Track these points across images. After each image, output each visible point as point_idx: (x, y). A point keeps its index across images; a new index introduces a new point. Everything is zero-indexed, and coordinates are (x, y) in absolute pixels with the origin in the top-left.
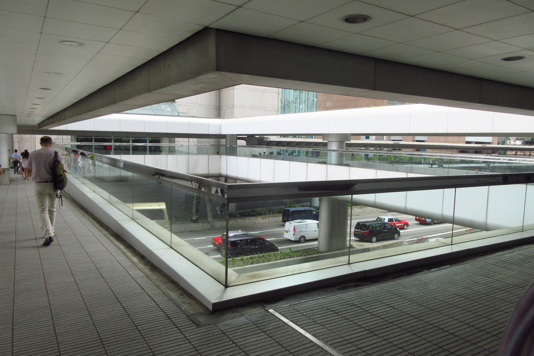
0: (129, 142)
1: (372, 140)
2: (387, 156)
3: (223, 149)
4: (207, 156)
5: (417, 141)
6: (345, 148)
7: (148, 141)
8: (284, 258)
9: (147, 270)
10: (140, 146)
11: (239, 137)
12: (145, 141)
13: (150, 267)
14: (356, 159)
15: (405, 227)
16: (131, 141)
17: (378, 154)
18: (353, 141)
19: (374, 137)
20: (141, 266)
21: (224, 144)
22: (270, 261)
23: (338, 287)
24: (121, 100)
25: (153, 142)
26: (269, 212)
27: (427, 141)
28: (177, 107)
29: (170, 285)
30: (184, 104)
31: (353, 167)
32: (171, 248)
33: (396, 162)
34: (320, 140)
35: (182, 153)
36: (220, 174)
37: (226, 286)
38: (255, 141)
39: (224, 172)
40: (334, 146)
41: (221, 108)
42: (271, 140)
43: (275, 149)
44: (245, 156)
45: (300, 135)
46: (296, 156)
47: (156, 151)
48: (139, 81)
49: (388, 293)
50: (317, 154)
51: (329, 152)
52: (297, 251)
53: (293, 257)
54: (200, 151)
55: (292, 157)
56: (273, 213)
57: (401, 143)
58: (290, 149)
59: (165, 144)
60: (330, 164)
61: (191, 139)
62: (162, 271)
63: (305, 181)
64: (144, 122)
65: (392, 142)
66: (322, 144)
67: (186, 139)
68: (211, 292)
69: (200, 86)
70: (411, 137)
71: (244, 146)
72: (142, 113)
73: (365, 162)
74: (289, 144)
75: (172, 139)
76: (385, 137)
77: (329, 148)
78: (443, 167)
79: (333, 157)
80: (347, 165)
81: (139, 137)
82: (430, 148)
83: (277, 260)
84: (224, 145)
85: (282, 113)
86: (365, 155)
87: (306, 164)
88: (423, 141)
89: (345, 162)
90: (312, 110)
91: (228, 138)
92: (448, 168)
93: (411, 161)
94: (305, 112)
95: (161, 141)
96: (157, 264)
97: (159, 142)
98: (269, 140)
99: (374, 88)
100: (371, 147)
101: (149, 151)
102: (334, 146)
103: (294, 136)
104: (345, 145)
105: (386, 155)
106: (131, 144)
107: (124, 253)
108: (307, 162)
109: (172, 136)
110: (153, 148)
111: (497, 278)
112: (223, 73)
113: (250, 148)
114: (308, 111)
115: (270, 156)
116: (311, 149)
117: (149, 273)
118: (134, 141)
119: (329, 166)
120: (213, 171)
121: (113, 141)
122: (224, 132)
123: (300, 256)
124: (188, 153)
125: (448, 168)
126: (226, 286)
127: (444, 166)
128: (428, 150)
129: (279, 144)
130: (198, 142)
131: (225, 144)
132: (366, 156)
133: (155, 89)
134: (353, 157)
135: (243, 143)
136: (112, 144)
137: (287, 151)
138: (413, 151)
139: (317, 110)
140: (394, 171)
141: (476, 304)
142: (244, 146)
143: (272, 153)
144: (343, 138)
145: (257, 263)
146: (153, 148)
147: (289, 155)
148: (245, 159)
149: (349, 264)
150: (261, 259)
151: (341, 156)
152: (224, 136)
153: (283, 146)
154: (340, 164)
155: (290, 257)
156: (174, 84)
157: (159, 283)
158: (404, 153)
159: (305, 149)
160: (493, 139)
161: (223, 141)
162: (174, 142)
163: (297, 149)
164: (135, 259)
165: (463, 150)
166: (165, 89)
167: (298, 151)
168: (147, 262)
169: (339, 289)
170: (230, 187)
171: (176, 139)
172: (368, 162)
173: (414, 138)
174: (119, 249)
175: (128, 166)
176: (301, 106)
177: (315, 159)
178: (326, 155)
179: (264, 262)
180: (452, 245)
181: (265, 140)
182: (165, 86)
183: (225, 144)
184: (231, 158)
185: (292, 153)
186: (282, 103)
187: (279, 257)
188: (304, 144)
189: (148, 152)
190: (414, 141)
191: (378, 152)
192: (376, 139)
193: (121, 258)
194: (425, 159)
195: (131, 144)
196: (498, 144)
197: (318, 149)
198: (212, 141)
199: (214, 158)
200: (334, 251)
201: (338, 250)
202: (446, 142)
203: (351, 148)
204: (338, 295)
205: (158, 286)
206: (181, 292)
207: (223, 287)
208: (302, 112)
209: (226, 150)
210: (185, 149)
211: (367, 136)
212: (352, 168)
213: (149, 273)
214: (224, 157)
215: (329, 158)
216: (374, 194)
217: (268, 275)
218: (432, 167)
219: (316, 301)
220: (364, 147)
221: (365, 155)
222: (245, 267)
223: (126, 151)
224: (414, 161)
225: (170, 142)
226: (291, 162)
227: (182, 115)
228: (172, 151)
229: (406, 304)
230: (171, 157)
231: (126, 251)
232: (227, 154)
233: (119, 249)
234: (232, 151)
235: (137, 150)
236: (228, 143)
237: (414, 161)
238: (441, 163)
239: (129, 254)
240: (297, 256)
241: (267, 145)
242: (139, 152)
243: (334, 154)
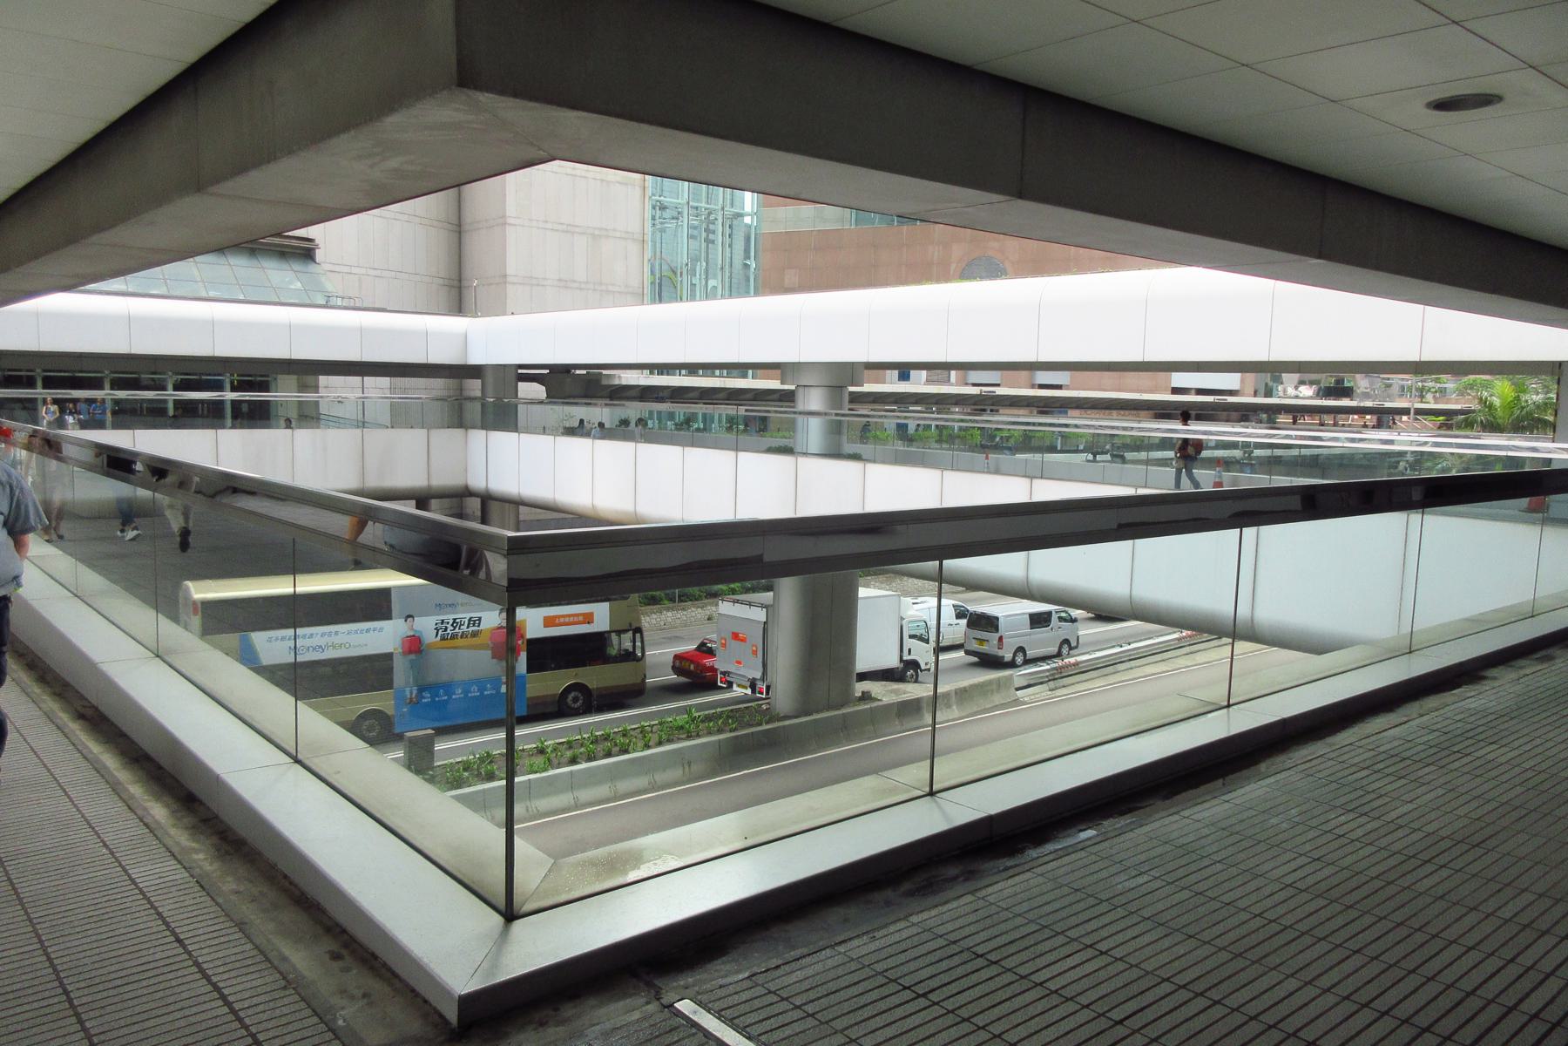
0: (164, 389)
1: (919, 384)
2: (961, 429)
3: (473, 410)
4: (424, 431)
5: (1042, 386)
6: (846, 405)
7: (228, 386)
8: (670, 741)
9: (202, 857)
10: (202, 401)
11: (523, 373)
12: (218, 386)
13: (215, 839)
14: (876, 437)
15: (1065, 650)
16: (170, 386)
17: (934, 423)
18: (868, 388)
19: (924, 373)
20: (180, 837)
21: (477, 396)
22: (626, 752)
23: (906, 886)
24: (99, 228)
25: (246, 390)
27: (1068, 388)
28: (323, 279)
29: (291, 915)
30: (346, 269)
31: (874, 462)
32: (297, 761)
33: (989, 447)
34: (774, 384)
35: (339, 422)
36: (467, 487)
37: (510, 915)
38: (576, 386)
39: (477, 482)
40: (814, 400)
41: (465, 283)
43: (633, 410)
44: (544, 431)
45: (709, 368)
46: (698, 430)
47: (255, 416)
48: (160, 149)
49: (1079, 895)
50: (761, 425)
51: (800, 419)
52: (708, 719)
53: (698, 736)
54: (401, 417)
55: (688, 432)
57: (1000, 391)
58: (681, 410)
59: (283, 394)
60: (805, 454)
61: (370, 381)
62: (260, 854)
63: (792, 515)
64: (212, 325)
65: (975, 391)
66: (776, 396)
67: (355, 380)
68: (455, 949)
69: (394, 163)
70: (1024, 374)
71: (541, 402)
72: (204, 294)
73: (900, 446)
74: (678, 394)
75: (310, 379)
76: (953, 373)
78: (1123, 460)
79: (813, 432)
80: (855, 457)
81: (198, 372)
82: (1077, 407)
83: (647, 746)
84: (475, 399)
85: (653, 302)
86: (899, 425)
87: (733, 454)
88: (1059, 387)
89: (849, 448)
90: (746, 294)
91: (490, 378)
92: (1148, 462)
93: (1028, 443)
94: (723, 297)
95: (273, 386)
96: (243, 832)
97: (264, 387)
98: (616, 382)
99: (1021, 192)
100: (916, 403)
102: (814, 400)
103: (692, 369)
104: (846, 398)
105: (956, 425)
106: (171, 395)
107: (116, 788)
108: (737, 450)
109: (309, 370)
110: (245, 408)
111: (1393, 815)
112: (485, 98)
113: (556, 407)
114: (730, 296)
115: (621, 431)
116: (745, 409)
117: (208, 867)
118: (181, 386)
119: (802, 460)
120: (444, 478)
121: (107, 385)
122: (475, 359)
123: (720, 731)
124: (362, 424)
125: (1148, 462)
126: (510, 915)
127: (1129, 455)
128: (1071, 413)
129: (646, 394)
130: (392, 389)
131: (479, 394)
132: (902, 428)
133: (218, 180)
134: (865, 432)
135: (536, 390)
136: (104, 394)
137: (671, 416)
138: (1031, 414)
139: (757, 294)
140: (989, 473)
141: (1367, 920)
142: (541, 402)
143: (625, 422)
144: (841, 377)
145: (590, 759)
146: (245, 408)
147: (679, 427)
148: (546, 440)
149: (932, 793)
150: (600, 747)
151: (835, 429)
152: (476, 371)
153: (661, 400)
154: (834, 453)
155: (689, 737)
156: (290, 152)
157: (248, 911)
158: (1003, 419)
159: (730, 410)
160: (1242, 381)
161: (474, 387)
162: (316, 388)
163: (700, 409)
164: (159, 812)
165: (1162, 411)
166: (255, 175)
167: (704, 415)
168: (205, 821)
169: (910, 894)
170: (517, 547)
171: (323, 380)
172: (910, 446)
173: (1032, 378)
174: (100, 770)
175: (160, 470)
176: (712, 283)
177: (753, 439)
178: (791, 426)
179: (609, 755)
180: (1229, 706)
181: (604, 382)
182: (257, 164)
183: (479, 394)
184: (502, 440)
185: (688, 421)
186: (652, 273)
187: (655, 738)
188: (721, 395)
189: (229, 421)
190: (1033, 386)
191: (934, 418)
192: (929, 382)
193: (102, 807)
194: (1064, 436)
195: (171, 395)
196: (1255, 394)
197: (759, 409)
198: (438, 385)
199: (447, 438)
200: (818, 712)
201: (829, 708)
202: (1119, 390)
203: (866, 408)
204: (915, 919)
205: (241, 926)
206: (334, 947)
207: (498, 920)
208: (715, 298)
209: (483, 412)
210: (348, 411)
211: (905, 370)
212: (871, 467)
213: (208, 867)
214: (477, 436)
215: (800, 436)
216: (1023, 554)
217: (661, 853)
218: (1094, 461)
219: (841, 949)
220: (895, 403)
221: (899, 425)
222: (551, 772)
223: (154, 416)
224: (1034, 443)
225: (303, 387)
226: (687, 449)
227: (339, 302)
228: (308, 416)
229: (1147, 939)
230: (304, 437)
231: (123, 775)
232: (487, 425)
233: (100, 770)
234: (502, 417)
235: (188, 415)
236: (490, 390)
237: (1034, 443)
238: (1119, 450)
239: (136, 790)
240: (710, 733)
241: (611, 398)
242: (200, 420)
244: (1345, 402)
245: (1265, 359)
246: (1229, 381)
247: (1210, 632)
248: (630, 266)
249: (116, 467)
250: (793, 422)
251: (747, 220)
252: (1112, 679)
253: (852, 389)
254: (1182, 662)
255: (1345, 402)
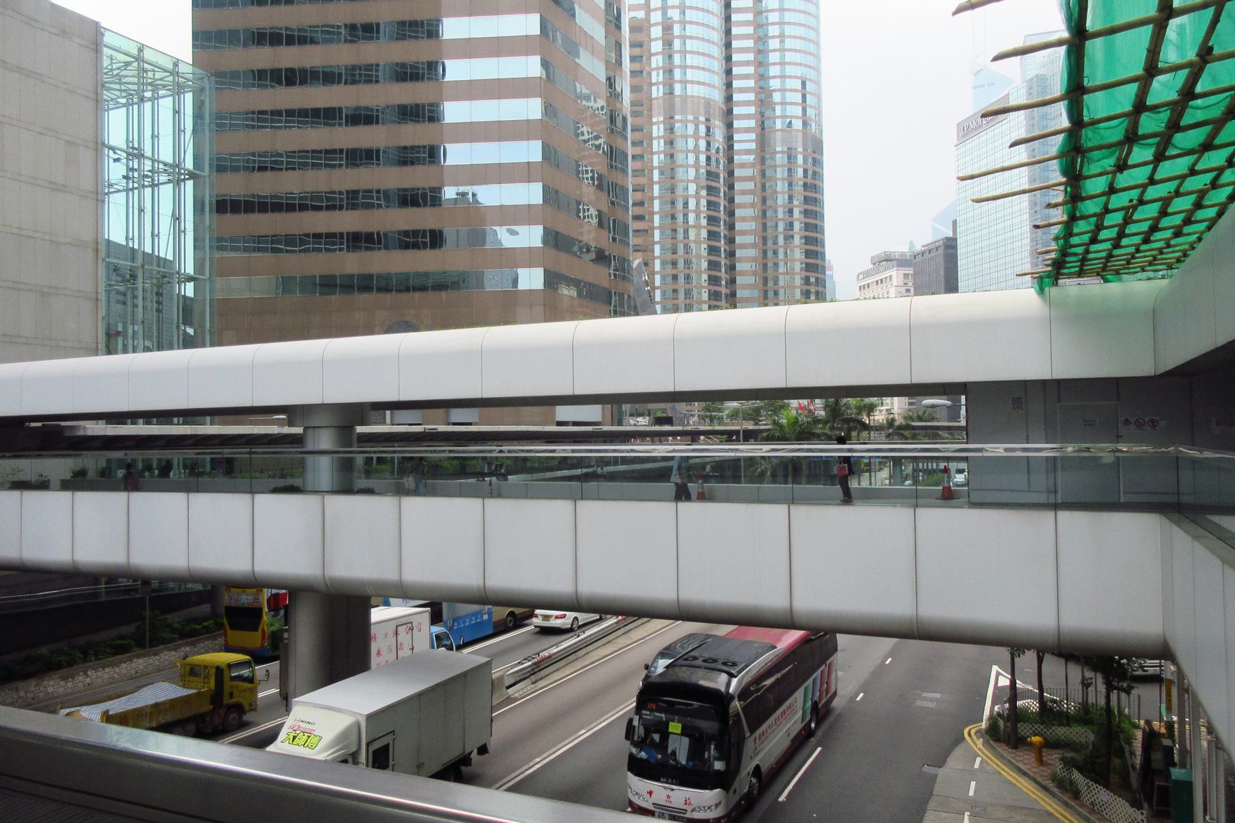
17: (375, 456)
26: (85, 653)
27: (477, 424)
40: (325, 440)
42: (90, 433)
51: (310, 458)
56: (96, 655)
70: (441, 411)
77: (310, 447)
79: (323, 470)
88: (470, 424)
98: (81, 433)
101: (808, 476)
103: (149, 416)
130: (910, 404)
138: (721, 442)
139: (212, 345)
151: (346, 466)
159: (191, 454)
173: (448, 415)
197: (227, 452)
215: (310, 475)
226: (193, 496)
243: (325, 462)
244: (666, 428)
245: (671, 389)
246: (592, 413)
247: (634, 615)
248: (89, 324)
249: (820, 282)
250: (302, 464)
251: (189, 290)
252: (579, 664)
253: (360, 429)
254: (623, 641)
255: (666, 428)
